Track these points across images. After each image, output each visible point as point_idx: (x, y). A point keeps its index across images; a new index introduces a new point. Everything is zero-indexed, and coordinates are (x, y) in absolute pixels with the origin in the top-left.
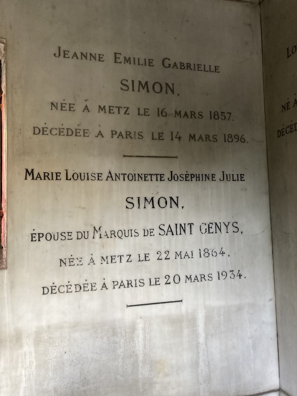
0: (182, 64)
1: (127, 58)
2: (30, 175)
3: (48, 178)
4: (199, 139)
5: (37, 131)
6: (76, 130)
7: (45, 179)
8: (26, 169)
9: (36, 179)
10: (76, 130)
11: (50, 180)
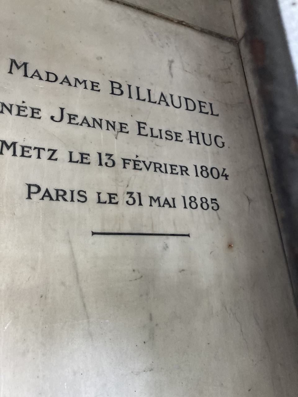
3: (160, 170)
4: (164, 203)
7: (57, 199)
11: (53, 200)
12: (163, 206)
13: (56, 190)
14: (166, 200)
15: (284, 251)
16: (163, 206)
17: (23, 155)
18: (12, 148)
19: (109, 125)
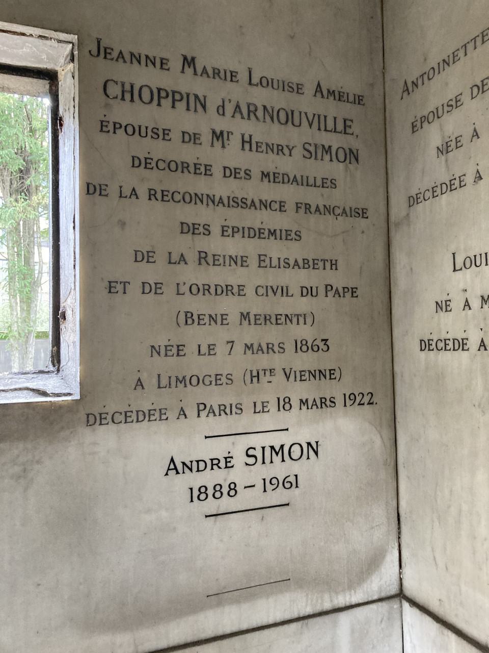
0: (306, 261)
1: (326, 147)
2: (304, 404)
5: (187, 138)
6: (146, 159)
9: (311, 408)
10: (146, 159)
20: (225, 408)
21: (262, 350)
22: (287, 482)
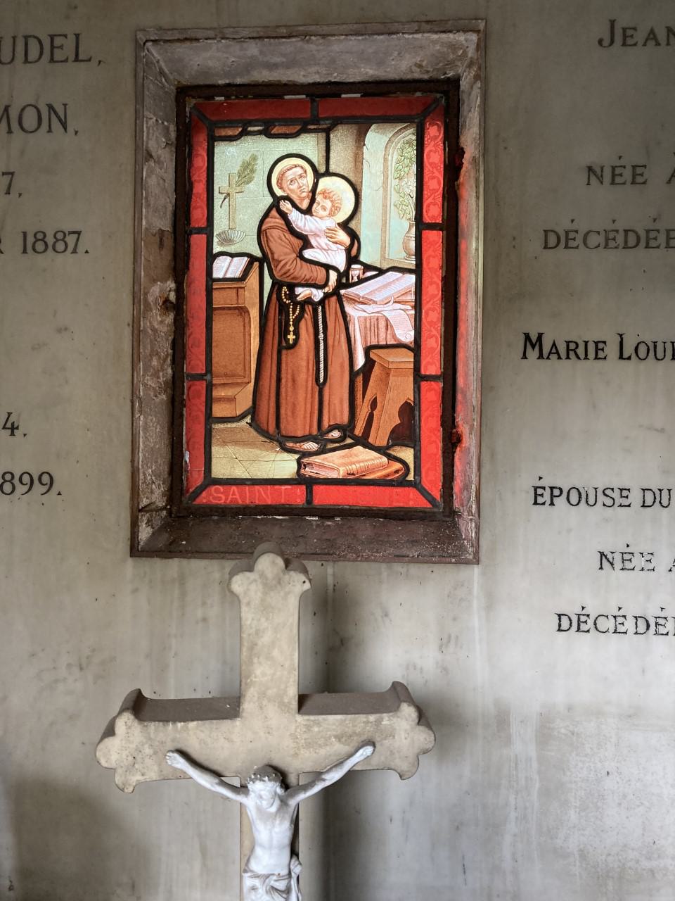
3: (576, 354)
4: (550, 353)
8: (525, 334)
12: (548, 358)
13: (50, 36)
14: (533, 348)
15: (419, 415)
16: (548, 358)
17: (596, 358)
18: (537, 348)
19: (62, 115)
20: (577, 347)
21: (557, 353)
22: (46, 484)
